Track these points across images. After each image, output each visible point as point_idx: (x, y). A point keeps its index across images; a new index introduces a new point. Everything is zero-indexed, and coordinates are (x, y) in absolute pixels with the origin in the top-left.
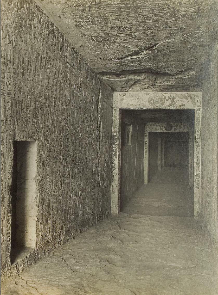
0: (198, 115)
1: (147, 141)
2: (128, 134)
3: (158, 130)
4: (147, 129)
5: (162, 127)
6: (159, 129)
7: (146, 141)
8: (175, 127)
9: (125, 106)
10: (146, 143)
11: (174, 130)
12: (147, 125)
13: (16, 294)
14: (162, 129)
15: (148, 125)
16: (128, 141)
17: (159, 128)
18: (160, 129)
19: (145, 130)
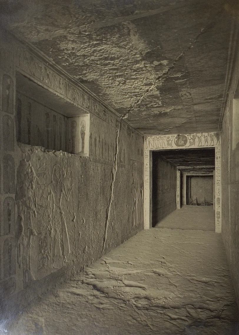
0: (218, 154)
1: (148, 164)
2: (83, 134)
3: (164, 146)
4: (148, 146)
5: (170, 142)
6: (167, 145)
7: (147, 165)
8: (192, 141)
9: (154, 149)
10: (147, 167)
11: (190, 146)
12: (147, 140)
13: (238, 163)
14: (171, 145)
15: (149, 139)
16: (83, 147)
17: (166, 143)
18: (168, 144)
19: (145, 148)
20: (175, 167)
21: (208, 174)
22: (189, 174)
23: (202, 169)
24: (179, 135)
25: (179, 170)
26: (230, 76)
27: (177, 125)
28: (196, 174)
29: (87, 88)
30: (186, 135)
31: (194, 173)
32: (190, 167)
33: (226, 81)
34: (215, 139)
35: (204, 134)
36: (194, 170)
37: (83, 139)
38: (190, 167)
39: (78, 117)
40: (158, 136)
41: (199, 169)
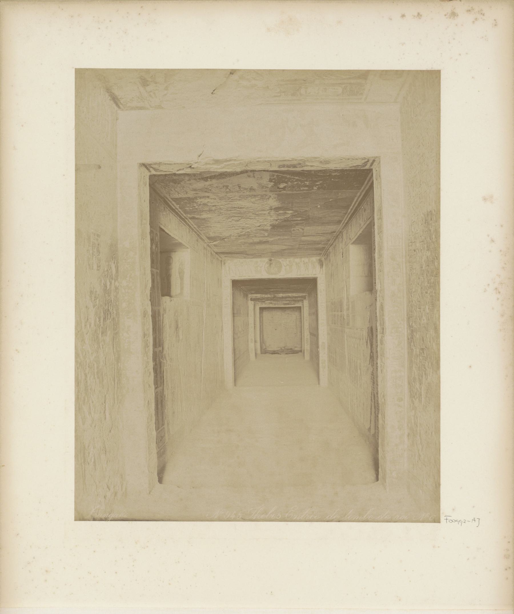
16: (182, 289)
20: (247, 296)
21: (294, 304)
22: (264, 306)
23: (286, 297)
24: (271, 260)
25: (251, 300)
26: (346, 221)
27: (274, 251)
28: (275, 304)
29: (195, 226)
30: (280, 260)
31: (271, 303)
32: (269, 296)
33: (363, 188)
34: (318, 266)
35: (303, 259)
36: (274, 299)
37: (182, 278)
38: (269, 296)
39: (175, 252)
40: (241, 260)
41: (283, 298)
